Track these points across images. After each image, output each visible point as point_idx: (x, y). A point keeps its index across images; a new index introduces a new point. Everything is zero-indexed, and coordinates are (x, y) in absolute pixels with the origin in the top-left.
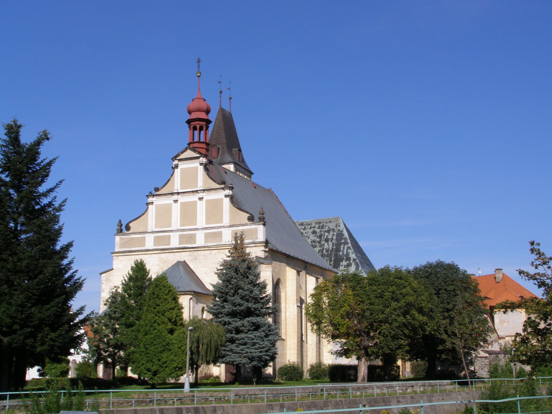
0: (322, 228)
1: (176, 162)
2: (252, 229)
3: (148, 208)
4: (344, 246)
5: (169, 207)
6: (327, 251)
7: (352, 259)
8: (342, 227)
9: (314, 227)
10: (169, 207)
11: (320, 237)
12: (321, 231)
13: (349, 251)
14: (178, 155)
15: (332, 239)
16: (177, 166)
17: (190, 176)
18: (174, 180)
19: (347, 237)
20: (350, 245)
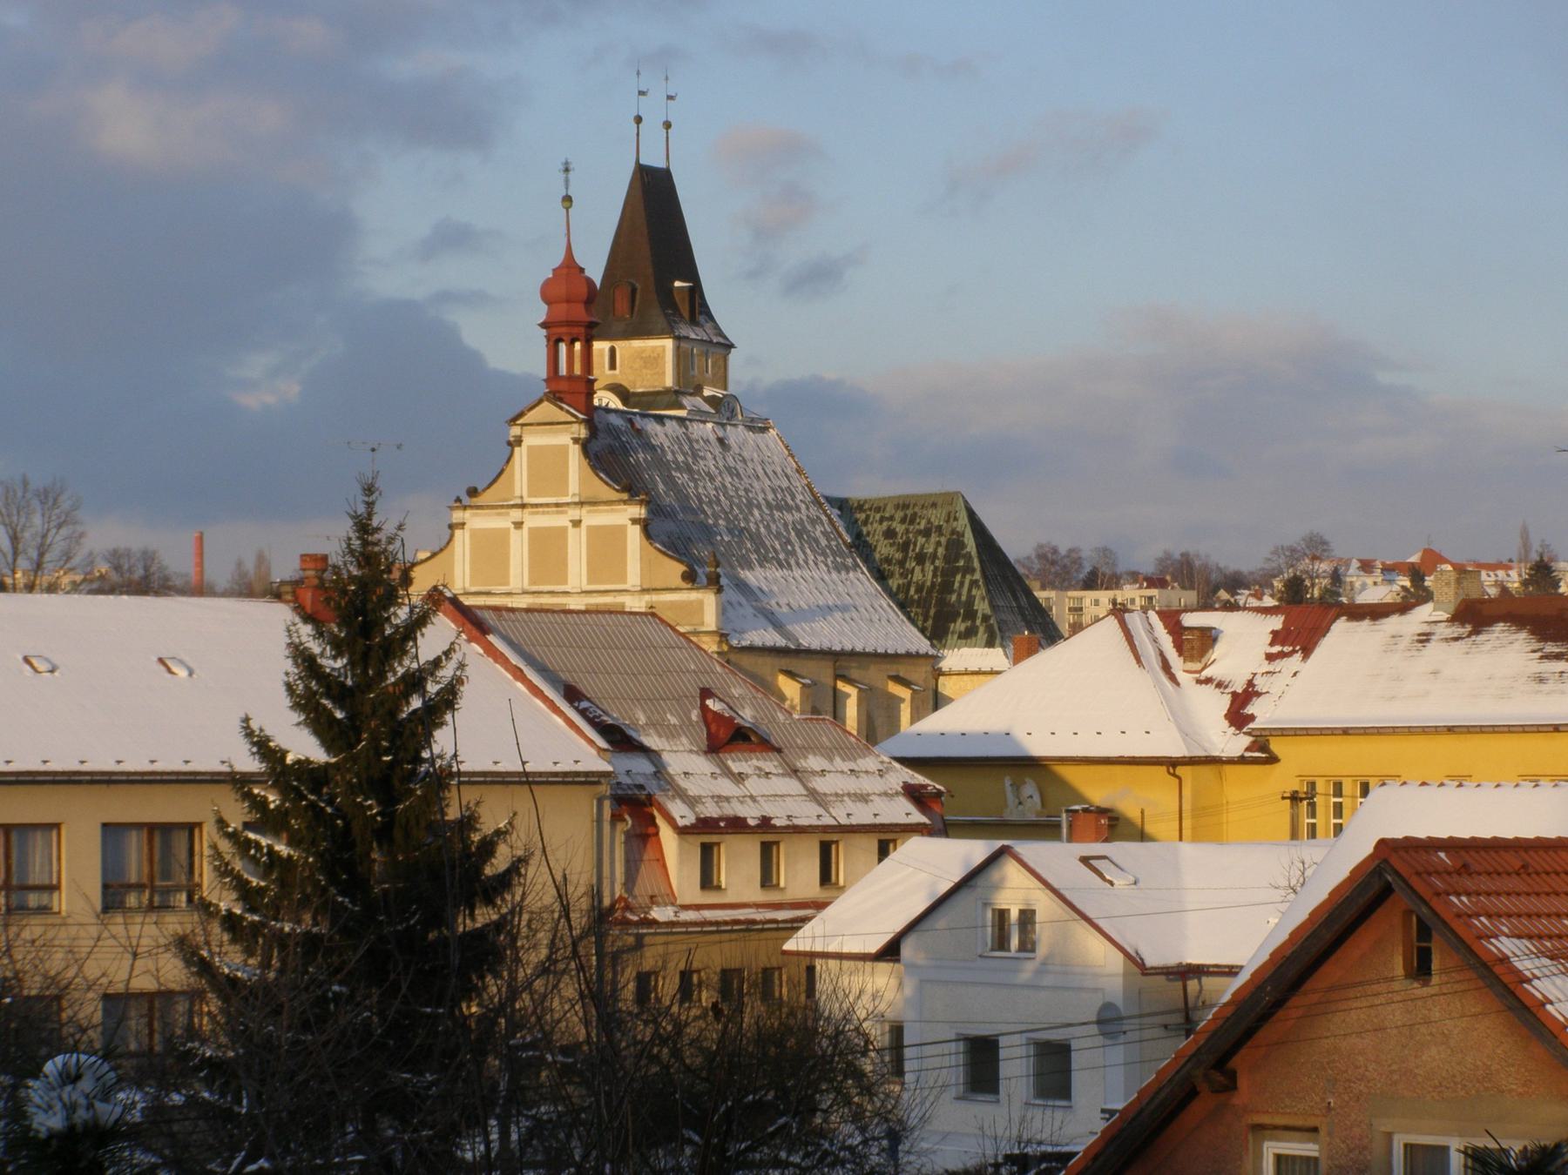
0: (912, 522)
1: (515, 431)
2: (691, 602)
3: (452, 537)
4: (964, 577)
5: (501, 538)
6: (919, 589)
7: (980, 615)
8: (963, 523)
9: (892, 518)
10: (501, 538)
11: (905, 547)
12: (907, 531)
13: (974, 592)
14: (521, 415)
15: (934, 556)
16: (519, 441)
17: (547, 463)
18: (513, 475)
19: (974, 552)
20: (977, 576)
